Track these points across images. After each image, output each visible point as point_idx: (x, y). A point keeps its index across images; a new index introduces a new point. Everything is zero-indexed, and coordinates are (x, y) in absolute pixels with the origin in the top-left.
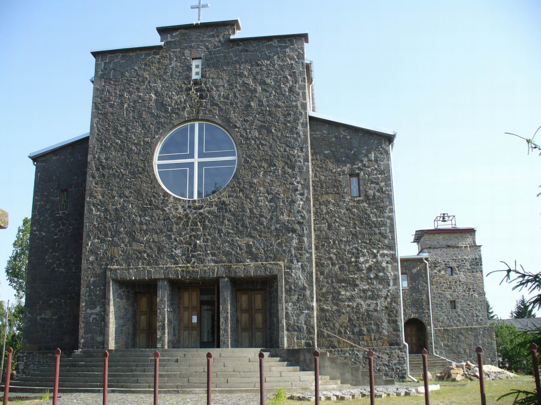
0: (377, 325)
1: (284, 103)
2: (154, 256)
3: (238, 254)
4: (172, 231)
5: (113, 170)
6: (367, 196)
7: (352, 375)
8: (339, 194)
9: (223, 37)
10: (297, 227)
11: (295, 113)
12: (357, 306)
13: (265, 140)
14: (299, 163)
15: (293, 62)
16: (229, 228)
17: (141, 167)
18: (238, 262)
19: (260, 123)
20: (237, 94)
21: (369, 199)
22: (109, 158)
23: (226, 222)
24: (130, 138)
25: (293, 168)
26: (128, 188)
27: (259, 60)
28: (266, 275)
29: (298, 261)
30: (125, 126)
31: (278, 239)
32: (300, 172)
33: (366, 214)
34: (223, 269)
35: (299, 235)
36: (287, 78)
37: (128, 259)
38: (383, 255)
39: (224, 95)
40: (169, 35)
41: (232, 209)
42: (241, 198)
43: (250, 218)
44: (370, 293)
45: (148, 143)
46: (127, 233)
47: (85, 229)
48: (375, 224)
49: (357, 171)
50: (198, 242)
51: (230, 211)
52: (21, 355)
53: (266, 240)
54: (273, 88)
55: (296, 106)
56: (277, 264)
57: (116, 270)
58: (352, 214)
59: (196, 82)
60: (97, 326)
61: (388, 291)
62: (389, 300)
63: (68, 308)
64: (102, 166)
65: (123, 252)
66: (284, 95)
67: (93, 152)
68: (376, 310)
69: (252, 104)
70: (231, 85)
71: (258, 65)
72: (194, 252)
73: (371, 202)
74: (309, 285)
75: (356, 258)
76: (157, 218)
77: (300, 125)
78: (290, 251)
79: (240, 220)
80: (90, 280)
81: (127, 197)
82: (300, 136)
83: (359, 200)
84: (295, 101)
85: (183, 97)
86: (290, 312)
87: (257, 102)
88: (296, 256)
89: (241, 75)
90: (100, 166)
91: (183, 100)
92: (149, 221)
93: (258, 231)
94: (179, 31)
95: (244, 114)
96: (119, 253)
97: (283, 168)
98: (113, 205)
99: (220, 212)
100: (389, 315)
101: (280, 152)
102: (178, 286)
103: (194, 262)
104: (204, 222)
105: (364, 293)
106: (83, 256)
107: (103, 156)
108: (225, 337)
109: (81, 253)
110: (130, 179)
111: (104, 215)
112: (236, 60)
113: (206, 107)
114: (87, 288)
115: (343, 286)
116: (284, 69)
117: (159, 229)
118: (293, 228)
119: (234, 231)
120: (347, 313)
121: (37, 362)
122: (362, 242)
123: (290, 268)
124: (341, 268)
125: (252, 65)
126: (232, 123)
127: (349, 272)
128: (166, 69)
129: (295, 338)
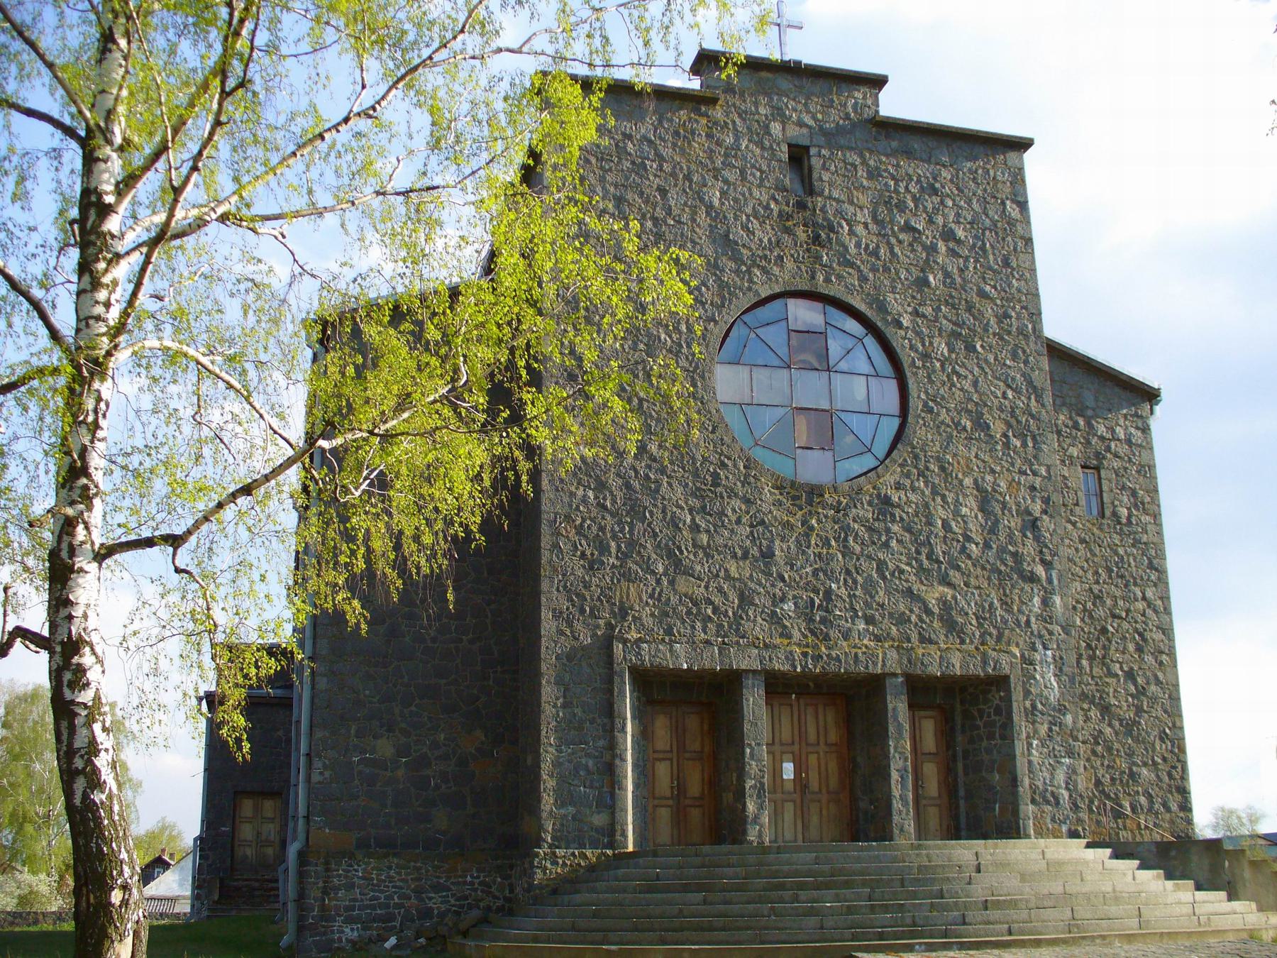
2: (730, 613)
13: (963, 365)
23: (894, 543)
48: (1135, 579)
53: (980, 595)
60: (591, 787)
63: (442, 736)
69: (931, 278)
73: (1125, 529)
76: (734, 518)
79: (923, 544)
87: (940, 276)
88: (1040, 636)
93: (963, 574)
96: (641, 599)
99: (878, 519)
101: (996, 397)
104: (845, 540)
106: (543, 599)
118: (1032, 572)
121: (363, 878)
129: (1048, 820)
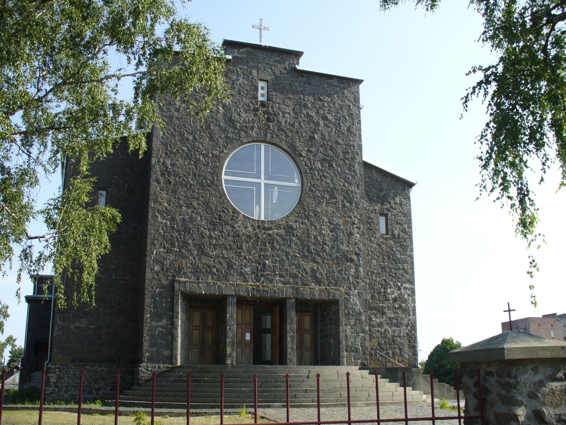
0: (400, 349)
1: (343, 141)
2: (223, 272)
3: (304, 277)
4: (242, 249)
5: (180, 178)
6: (393, 235)
7: (440, 390)
8: (371, 230)
9: (289, 65)
10: (355, 257)
11: (352, 153)
12: (385, 332)
13: (327, 173)
14: (356, 199)
15: (350, 104)
16: (295, 252)
17: (210, 180)
18: (303, 284)
19: (322, 156)
20: (302, 124)
21: (395, 238)
22: (176, 164)
23: (293, 245)
24: (198, 148)
25: (351, 202)
26: (196, 199)
27: (321, 95)
28: (329, 299)
29: (355, 289)
30: (192, 134)
31: (339, 267)
32: (357, 207)
33: (393, 251)
34: (291, 291)
35: (356, 265)
36: (345, 118)
37: (196, 271)
38: (406, 288)
39: (290, 122)
40: (236, 50)
41: (298, 234)
42: (307, 224)
43: (314, 244)
44: (395, 321)
45: (216, 156)
46: (195, 245)
47: (149, 236)
49: (386, 212)
50: (267, 262)
51: (297, 235)
52: (53, 367)
53: (328, 267)
54: (334, 124)
55: (353, 146)
56: (338, 290)
57: (185, 282)
58: (381, 249)
59: (263, 104)
61: (409, 320)
62: (409, 328)
64: (168, 172)
65: (191, 264)
66: (343, 134)
67: (157, 155)
68: (399, 336)
69: (316, 136)
70: (296, 113)
71: (320, 100)
72: (264, 271)
74: (364, 311)
75: (385, 289)
76: (227, 234)
77: (357, 165)
78: (348, 279)
79: (305, 246)
80: (155, 291)
81: (195, 209)
82: (356, 175)
83: (387, 238)
84: (353, 141)
85: (251, 117)
86: (348, 334)
87: (320, 135)
89: (305, 106)
90: (165, 172)
91: (251, 119)
92: (219, 236)
93: (322, 258)
94: (246, 49)
95: (308, 144)
96: (187, 265)
97: (343, 201)
98: (180, 215)
99: (287, 235)
100: (410, 341)
102: (242, 302)
103: (263, 282)
104: (273, 243)
105: (390, 320)
106: (147, 264)
107: (168, 162)
108: (292, 355)
109: (145, 262)
110: (198, 190)
111: (171, 224)
112: (300, 91)
113: (273, 131)
114: (152, 299)
115: (374, 314)
116: (344, 109)
117: (229, 245)
118: (351, 258)
119: (300, 255)
120: (377, 337)
121: (73, 374)
122: (389, 275)
123: (349, 295)
124: (373, 297)
125: (315, 99)
126: (297, 151)
127: (379, 301)
128: (233, 84)
